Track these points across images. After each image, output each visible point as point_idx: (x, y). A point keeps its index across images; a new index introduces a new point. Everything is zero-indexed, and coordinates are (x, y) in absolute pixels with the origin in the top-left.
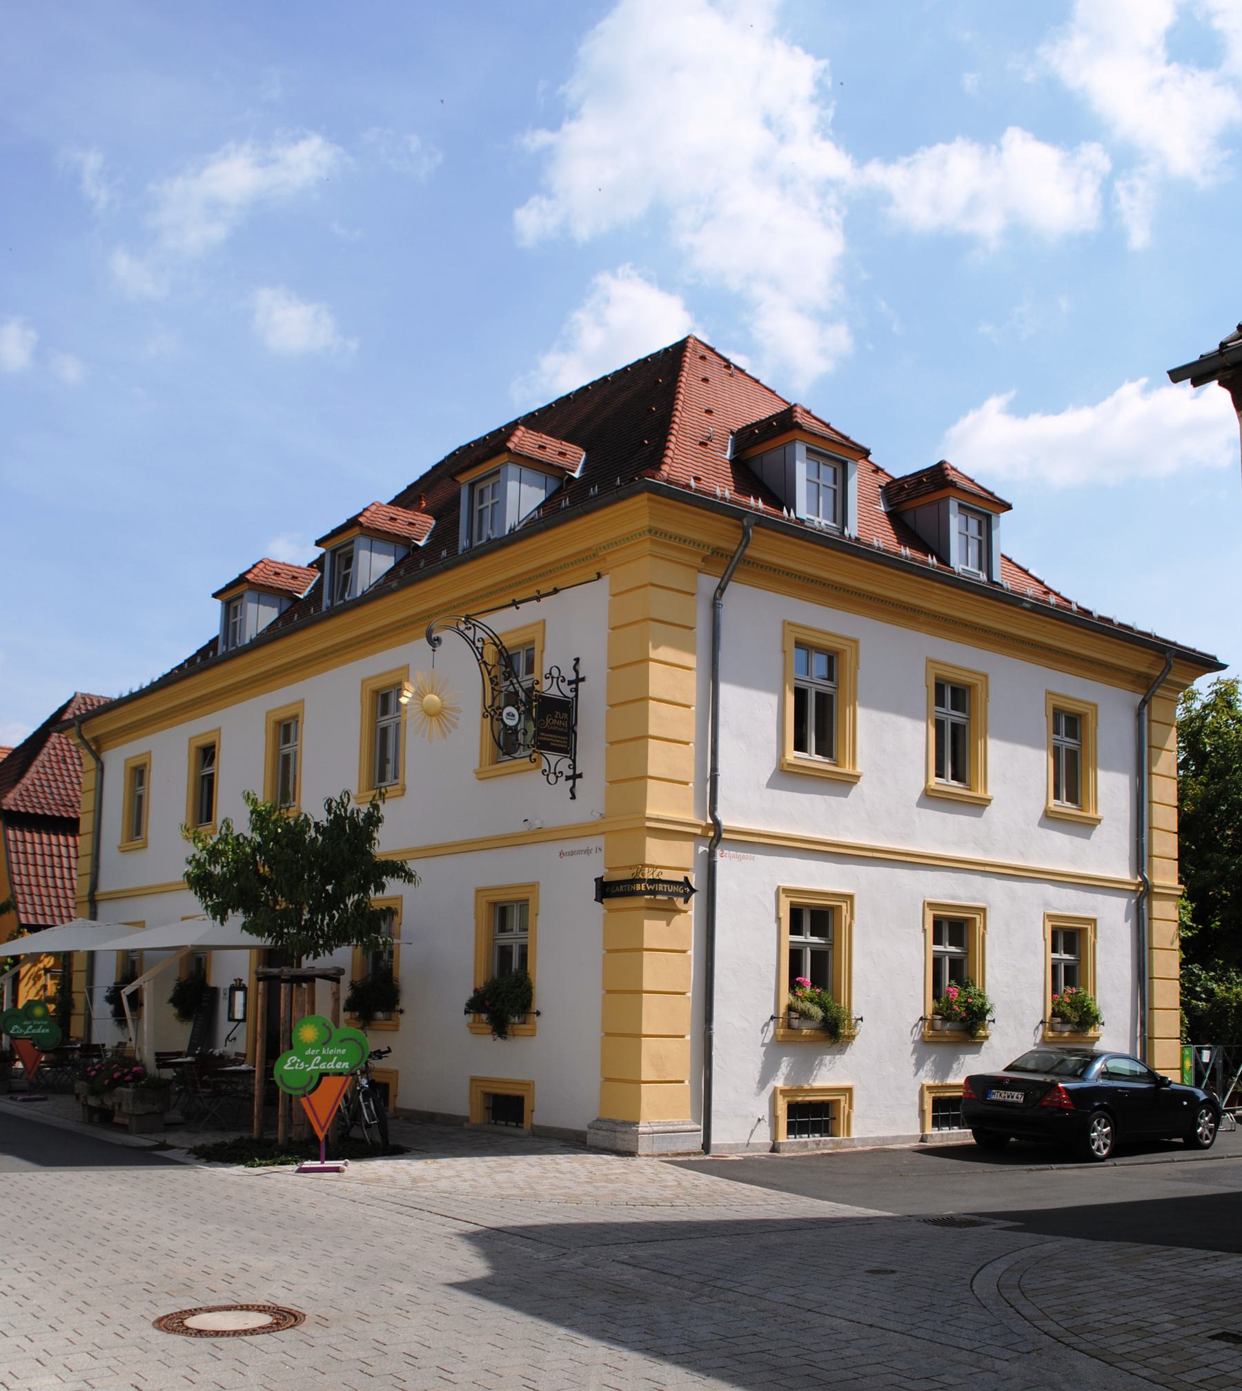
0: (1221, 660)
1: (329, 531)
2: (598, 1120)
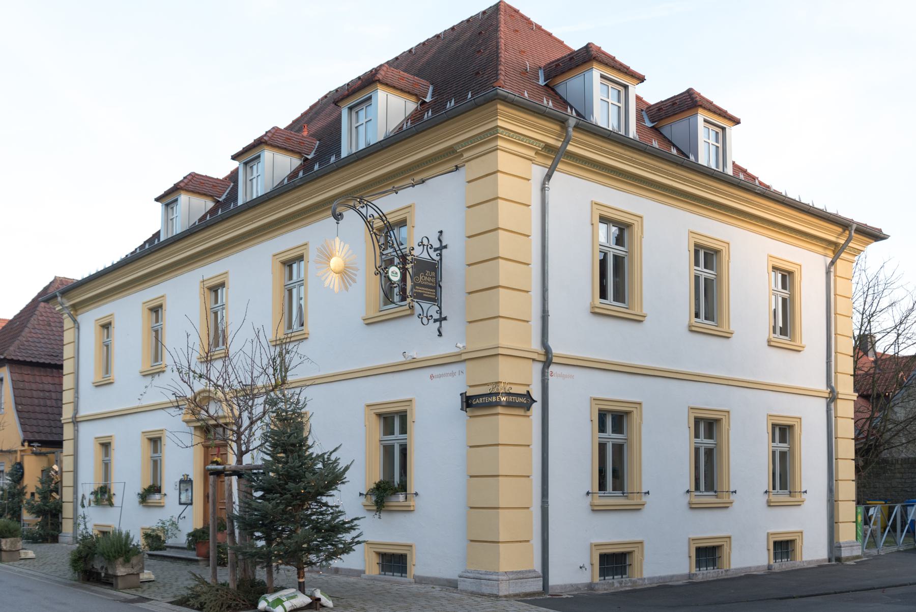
0: (884, 232)
1: (241, 149)
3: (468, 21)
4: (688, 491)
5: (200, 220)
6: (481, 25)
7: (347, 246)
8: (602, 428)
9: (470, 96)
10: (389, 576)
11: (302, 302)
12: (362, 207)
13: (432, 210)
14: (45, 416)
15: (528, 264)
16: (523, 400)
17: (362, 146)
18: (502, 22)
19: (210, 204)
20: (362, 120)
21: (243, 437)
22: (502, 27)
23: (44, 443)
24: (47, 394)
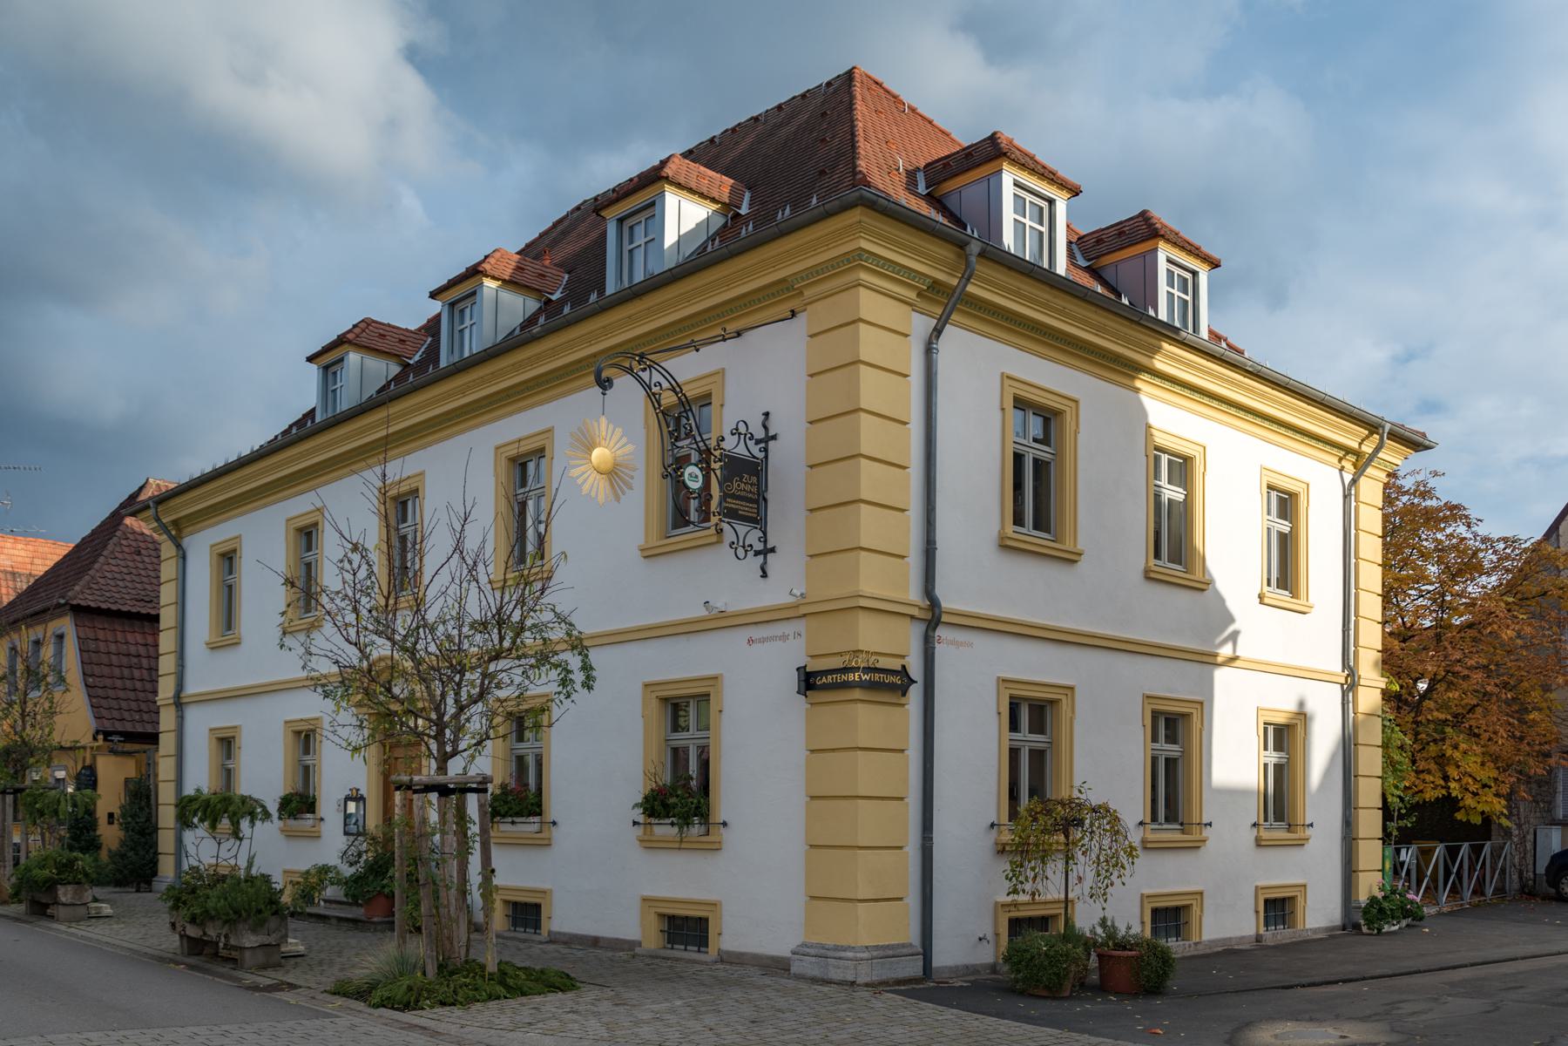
2: (804, 945)
3: (803, 96)
4: (1141, 823)
5: (378, 392)
6: (823, 103)
7: (619, 431)
8: (1014, 726)
9: (814, 201)
10: (678, 952)
11: (334, 921)
12: (644, 370)
13: (757, 379)
14: (132, 695)
15: (905, 468)
16: (896, 680)
17: (639, 276)
18: (859, 97)
19: (395, 369)
20: (640, 239)
21: (448, 732)
22: (859, 106)
23: (129, 737)
24: (135, 660)
